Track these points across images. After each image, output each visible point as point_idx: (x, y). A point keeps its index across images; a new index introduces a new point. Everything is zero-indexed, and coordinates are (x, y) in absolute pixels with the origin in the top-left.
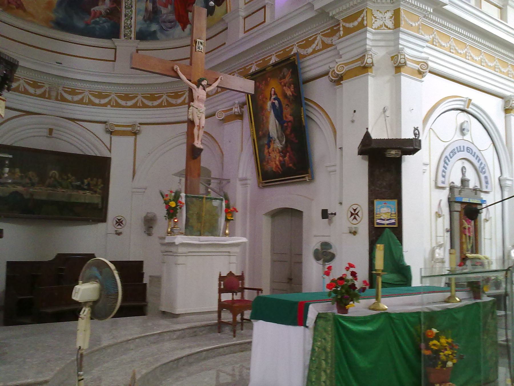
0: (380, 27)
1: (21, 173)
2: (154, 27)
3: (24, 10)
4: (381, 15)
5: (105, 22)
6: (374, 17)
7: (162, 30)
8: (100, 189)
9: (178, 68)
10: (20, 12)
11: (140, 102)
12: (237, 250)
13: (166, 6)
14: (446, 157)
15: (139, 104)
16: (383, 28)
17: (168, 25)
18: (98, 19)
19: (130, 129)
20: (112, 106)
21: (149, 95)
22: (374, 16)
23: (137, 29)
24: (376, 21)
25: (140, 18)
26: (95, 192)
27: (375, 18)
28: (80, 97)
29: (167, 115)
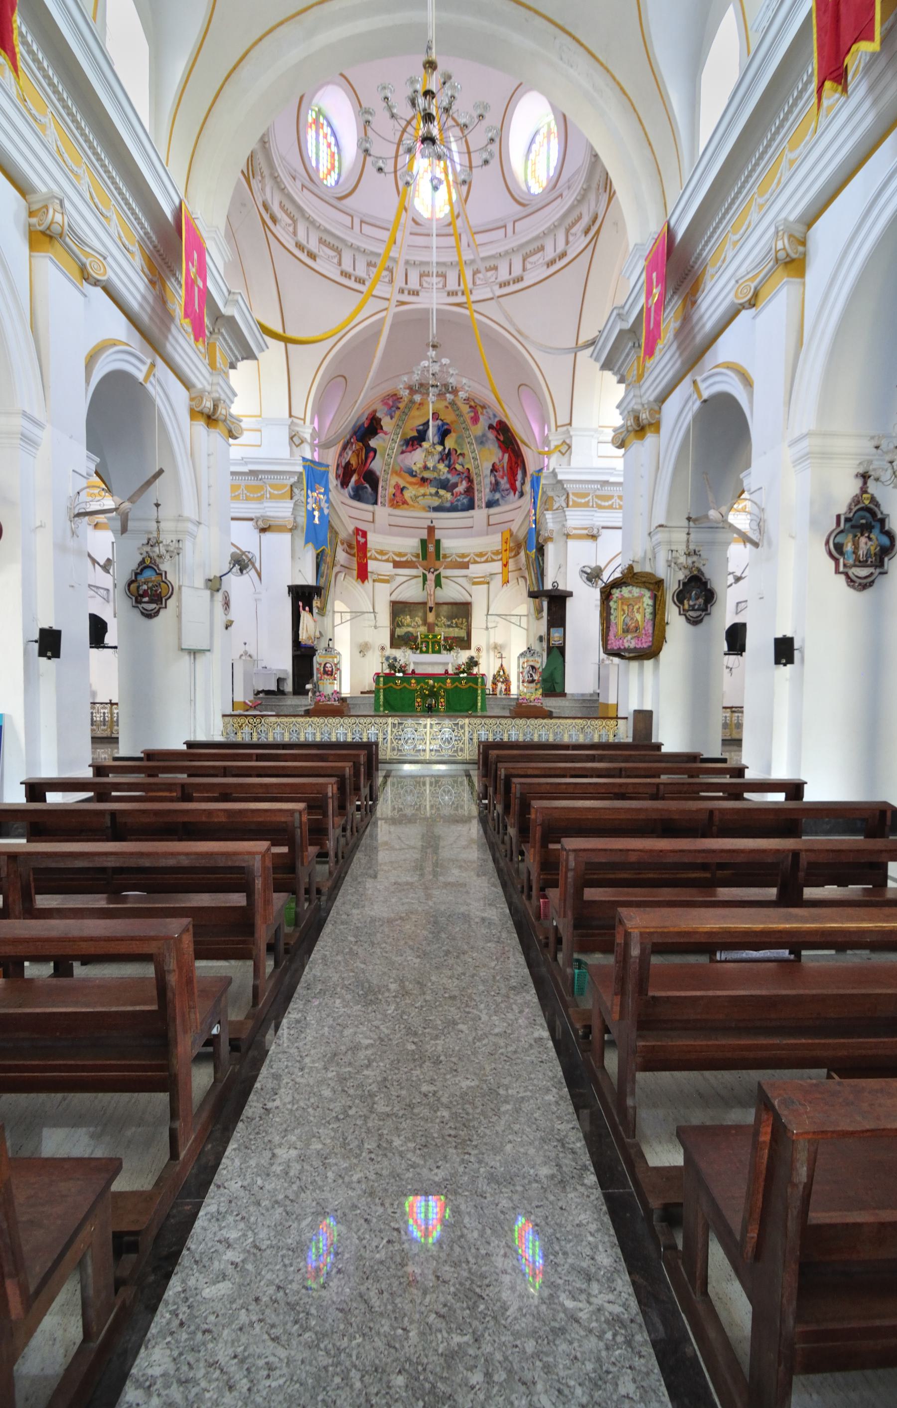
2: (497, 496)
7: (503, 497)
10: (405, 506)
13: (503, 478)
17: (506, 492)
25: (488, 490)
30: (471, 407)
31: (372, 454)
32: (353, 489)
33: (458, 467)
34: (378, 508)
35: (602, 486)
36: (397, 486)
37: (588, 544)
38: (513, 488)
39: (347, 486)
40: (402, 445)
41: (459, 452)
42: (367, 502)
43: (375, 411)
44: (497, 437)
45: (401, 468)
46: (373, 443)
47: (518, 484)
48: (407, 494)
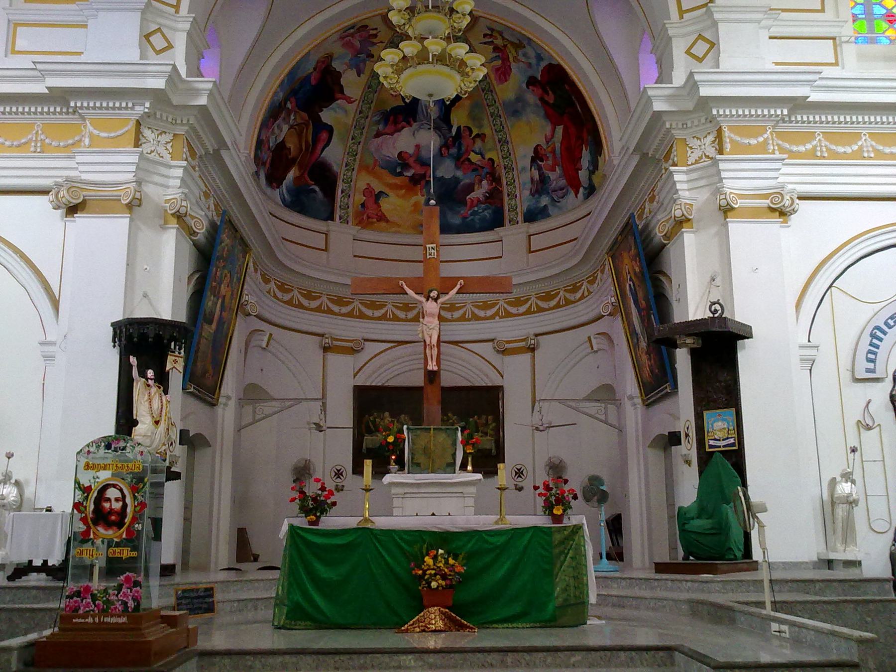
0: (699, 160)
1: (391, 417)
2: (545, 201)
3: (387, 221)
4: (699, 143)
5: (485, 209)
6: (689, 147)
8: (492, 430)
9: (404, 283)
10: (383, 224)
11: (534, 305)
12: (472, 489)
13: (553, 169)
14: (878, 328)
15: (534, 308)
16: (702, 161)
17: (560, 193)
18: (476, 209)
19: (523, 344)
20: (501, 318)
21: (514, 300)
22: (689, 146)
23: (525, 209)
24: (692, 152)
25: (527, 193)
26: (486, 434)
27: (691, 148)
28: (461, 312)
29: (546, 323)
30: (496, 49)
31: (324, 135)
32: (289, 190)
33: (474, 158)
34: (334, 227)
35: (792, 112)
36: (368, 191)
37: (771, 228)
38: (575, 184)
39: (279, 185)
40: (378, 122)
41: (475, 132)
42: (315, 216)
43: (329, 57)
44: (542, 99)
45: (376, 161)
46: (327, 116)
47: (583, 175)
48: (386, 205)
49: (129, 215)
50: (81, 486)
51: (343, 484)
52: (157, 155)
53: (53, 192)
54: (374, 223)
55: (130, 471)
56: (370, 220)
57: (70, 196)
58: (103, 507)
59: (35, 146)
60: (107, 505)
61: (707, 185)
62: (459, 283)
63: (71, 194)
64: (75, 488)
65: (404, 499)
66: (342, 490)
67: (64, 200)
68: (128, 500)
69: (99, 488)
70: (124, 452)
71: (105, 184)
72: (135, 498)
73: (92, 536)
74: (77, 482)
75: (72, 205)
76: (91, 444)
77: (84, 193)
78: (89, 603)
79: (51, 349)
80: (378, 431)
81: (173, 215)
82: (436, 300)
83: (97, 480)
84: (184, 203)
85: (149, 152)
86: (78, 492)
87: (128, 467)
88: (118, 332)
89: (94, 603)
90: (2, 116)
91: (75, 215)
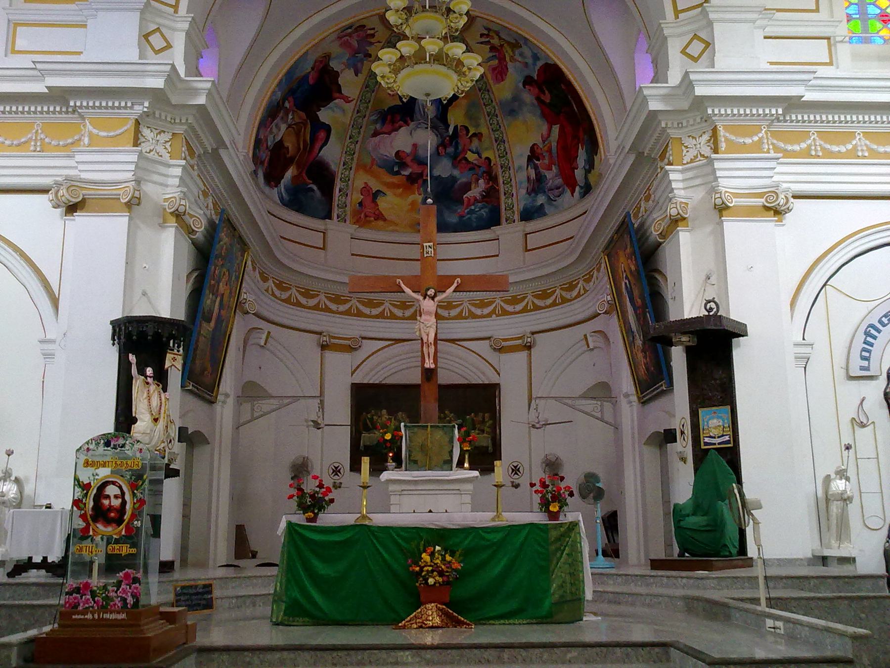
0: (694, 159)
1: (388, 415)
2: (541, 199)
3: (385, 220)
4: (694, 142)
5: (482, 208)
6: (685, 146)
8: (488, 427)
9: (401, 282)
10: (381, 223)
11: (530, 303)
12: (469, 487)
13: (549, 168)
14: (872, 326)
15: (530, 306)
16: (698, 160)
17: (556, 192)
18: (473, 207)
19: (519, 342)
20: (497, 316)
21: (510, 298)
22: (685, 145)
23: (521, 207)
24: (688, 151)
25: (523, 192)
26: (483, 431)
27: (686, 147)
28: (458, 310)
29: (543, 321)
30: (493, 48)
31: (322, 135)
32: (287, 189)
33: (471, 157)
34: (332, 225)
35: (786, 111)
36: (366, 190)
37: (766, 227)
38: (571, 183)
39: (277, 184)
40: (375, 122)
41: (472, 131)
42: (313, 215)
43: (327, 57)
44: (538, 99)
45: (373, 160)
46: (325, 115)
47: (579, 174)
48: (384, 204)
49: (129, 214)
50: (81, 483)
51: (341, 481)
52: (156, 154)
53: (53, 191)
54: (372, 221)
55: (129, 468)
56: (368, 219)
57: (69, 195)
58: (102, 504)
59: (35, 145)
60: (106, 502)
61: (703, 184)
62: (456, 281)
63: (70, 193)
64: (75, 485)
65: (402, 496)
66: (340, 487)
67: (63, 198)
68: (128, 497)
69: (98, 485)
70: (123, 449)
71: (105, 183)
72: (134, 495)
73: (91, 533)
74: (76, 479)
75: (71, 204)
76: (90, 441)
77: (84, 192)
78: (88, 599)
79: (50, 347)
80: (376, 428)
81: (171, 213)
82: (433, 298)
83: (97, 477)
84: (183, 202)
85: (148, 151)
86: (78, 489)
87: (127, 464)
88: (117, 330)
89: (93, 600)
90: (2, 116)
91: (75, 214)
